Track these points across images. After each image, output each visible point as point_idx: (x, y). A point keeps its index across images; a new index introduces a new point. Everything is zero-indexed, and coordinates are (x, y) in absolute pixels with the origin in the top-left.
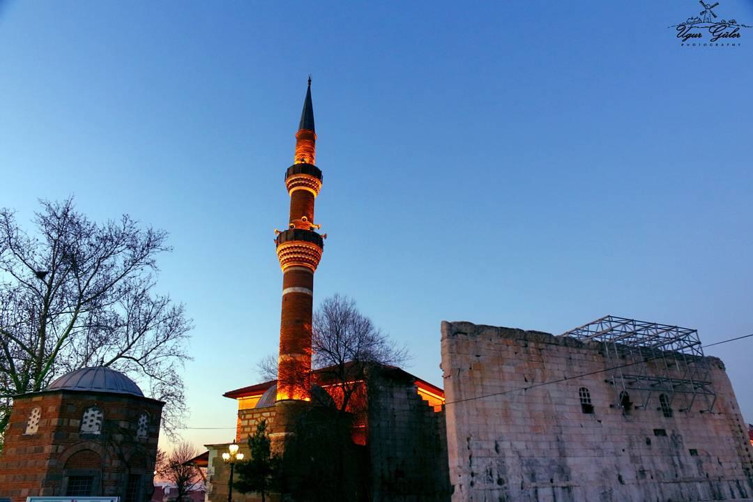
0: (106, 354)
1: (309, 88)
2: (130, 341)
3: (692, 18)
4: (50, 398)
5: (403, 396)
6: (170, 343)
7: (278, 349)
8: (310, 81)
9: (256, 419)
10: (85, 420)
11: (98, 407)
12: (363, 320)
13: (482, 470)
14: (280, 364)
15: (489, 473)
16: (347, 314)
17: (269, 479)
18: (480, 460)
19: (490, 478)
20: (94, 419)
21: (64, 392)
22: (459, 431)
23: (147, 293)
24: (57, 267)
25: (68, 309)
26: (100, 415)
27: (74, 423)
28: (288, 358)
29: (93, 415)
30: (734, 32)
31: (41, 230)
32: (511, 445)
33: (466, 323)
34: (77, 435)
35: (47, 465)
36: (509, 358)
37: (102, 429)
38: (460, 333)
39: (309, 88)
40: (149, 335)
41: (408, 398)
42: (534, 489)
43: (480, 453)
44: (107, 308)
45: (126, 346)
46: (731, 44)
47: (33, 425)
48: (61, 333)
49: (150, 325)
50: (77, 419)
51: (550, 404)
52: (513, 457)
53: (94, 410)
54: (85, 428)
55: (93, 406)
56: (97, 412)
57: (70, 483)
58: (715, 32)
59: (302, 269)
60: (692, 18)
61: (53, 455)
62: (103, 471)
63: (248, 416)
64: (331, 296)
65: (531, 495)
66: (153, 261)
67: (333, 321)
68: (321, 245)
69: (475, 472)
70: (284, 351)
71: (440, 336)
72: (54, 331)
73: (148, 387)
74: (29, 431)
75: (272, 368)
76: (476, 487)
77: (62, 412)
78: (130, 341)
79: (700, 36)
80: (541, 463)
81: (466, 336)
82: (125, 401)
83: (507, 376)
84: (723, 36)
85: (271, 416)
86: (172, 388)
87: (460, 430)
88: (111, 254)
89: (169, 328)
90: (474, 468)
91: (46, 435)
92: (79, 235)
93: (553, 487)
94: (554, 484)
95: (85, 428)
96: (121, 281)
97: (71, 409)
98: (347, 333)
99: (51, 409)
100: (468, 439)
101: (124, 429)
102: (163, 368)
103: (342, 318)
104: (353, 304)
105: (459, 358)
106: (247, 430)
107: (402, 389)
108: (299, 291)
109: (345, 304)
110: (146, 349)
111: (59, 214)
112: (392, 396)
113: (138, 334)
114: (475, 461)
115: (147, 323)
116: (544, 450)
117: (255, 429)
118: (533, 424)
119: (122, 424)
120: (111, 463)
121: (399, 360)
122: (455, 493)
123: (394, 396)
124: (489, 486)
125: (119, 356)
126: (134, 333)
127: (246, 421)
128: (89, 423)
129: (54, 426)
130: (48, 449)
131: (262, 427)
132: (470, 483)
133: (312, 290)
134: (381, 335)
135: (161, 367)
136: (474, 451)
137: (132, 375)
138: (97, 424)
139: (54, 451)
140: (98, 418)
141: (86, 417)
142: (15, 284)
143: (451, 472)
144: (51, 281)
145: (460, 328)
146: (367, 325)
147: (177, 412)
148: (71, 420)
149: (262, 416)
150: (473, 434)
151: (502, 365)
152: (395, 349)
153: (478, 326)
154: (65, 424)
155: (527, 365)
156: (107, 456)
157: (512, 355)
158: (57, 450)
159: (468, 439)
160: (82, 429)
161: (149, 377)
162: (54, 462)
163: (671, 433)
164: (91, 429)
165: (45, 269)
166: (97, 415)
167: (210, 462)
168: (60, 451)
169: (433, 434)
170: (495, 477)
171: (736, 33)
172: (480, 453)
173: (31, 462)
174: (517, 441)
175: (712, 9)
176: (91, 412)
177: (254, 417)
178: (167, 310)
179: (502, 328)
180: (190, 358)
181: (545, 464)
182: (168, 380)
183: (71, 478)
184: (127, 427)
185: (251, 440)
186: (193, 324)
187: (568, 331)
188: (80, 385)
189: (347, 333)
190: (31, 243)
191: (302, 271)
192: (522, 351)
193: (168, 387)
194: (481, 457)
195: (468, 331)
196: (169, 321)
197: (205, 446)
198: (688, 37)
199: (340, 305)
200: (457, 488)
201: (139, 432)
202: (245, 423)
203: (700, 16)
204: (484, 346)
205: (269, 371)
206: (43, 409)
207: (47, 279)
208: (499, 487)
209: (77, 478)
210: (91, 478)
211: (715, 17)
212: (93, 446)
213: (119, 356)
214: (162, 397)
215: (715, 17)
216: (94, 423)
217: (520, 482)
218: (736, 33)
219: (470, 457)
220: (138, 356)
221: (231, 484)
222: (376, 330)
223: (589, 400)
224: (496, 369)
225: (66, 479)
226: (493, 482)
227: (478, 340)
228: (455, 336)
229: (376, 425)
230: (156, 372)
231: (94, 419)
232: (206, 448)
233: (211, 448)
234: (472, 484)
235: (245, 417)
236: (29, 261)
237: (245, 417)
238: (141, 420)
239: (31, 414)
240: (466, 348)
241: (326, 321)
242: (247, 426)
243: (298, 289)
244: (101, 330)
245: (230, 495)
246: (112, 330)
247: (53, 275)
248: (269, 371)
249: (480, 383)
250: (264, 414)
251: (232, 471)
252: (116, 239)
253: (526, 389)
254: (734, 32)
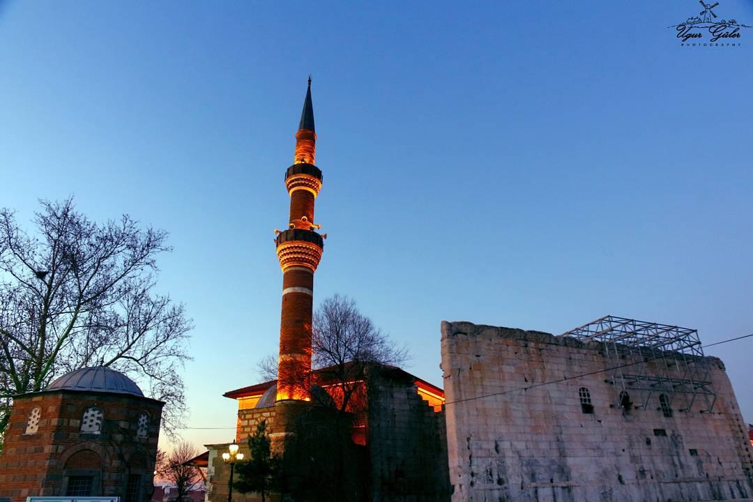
0: (106, 354)
1: (309, 88)
2: (130, 341)
3: (692, 18)
4: (50, 398)
5: (403, 396)
6: (170, 343)
7: (278, 349)
8: (310, 81)
9: (256, 419)
10: (85, 420)
11: (98, 407)
12: (363, 320)
13: (482, 470)
14: (280, 364)
15: (489, 473)
16: (347, 314)
17: (269, 479)
18: (480, 460)
19: (490, 478)
20: (94, 419)
21: (64, 392)
22: (459, 431)
23: (147, 293)
24: (57, 267)
25: (68, 309)
26: (100, 415)
27: (74, 423)
28: (288, 358)
29: (93, 415)
30: (734, 32)
31: (41, 230)
32: (511, 445)
33: (466, 323)
34: (77, 435)
35: (47, 465)
36: (509, 358)
37: (102, 429)
38: (460, 333)
39: (309, 88)
40: (149, 335)
41: (408, 398)
42: (534, 489)
43: (480, 453)
44: (107, 308)
45: (126, 346)
46: (731, 44)
47: (33, 425)
48: (61, 333)
49: (150, 325)
50: (77, 419)
51: (550, 404)
52: (513, 457)
53: (94, 410)
54: (85, 428)
55: (93, 406)
56: (97, 412)
57: (70, 483)
58: (715, 32)
59: (302, 269)
60: (692, 18)
61: (53, 455)
62: (103, 471)
63: (248, 416)
64: (331, 296)
65: (531, 495)
66: (153, 261)
67: (333, 321)
68: (321, 245)
69: (475, 472)
70: (284, 351)
71: (440, 336)
72: (54, 331)
73: (148, 387)
74: (29, 431)
75: (272, 368)
76: (476, 487)
77: (62, 412)
78: (130, 341)
79: (700, 36)
80: (541, 463)
81: (466, 336)
82: (125, 401)
83: (507, 376)
84: (723, 36)
85: (271, 416)
86: (172, 388)
87: (460, 430)
88: (111, 254)
89: (169, 328)
90: (474, 468)
91: (46, 435)
92: (79, 235)
95: (85, 428)
96: (121, 281)
97: (71, 409)
98: (347, 333)
99: (51, 409)
100: (468, 439)
101: (124, 429)
102: (163, 368)
103: (342, 318)
104: (353, 304)
105: (459, 358)
106: (247, 430)
107: (402, 389)
108: (299, 291)
109: (345, 304)
110: (146, 349)
111: (59, 214)
112: (392, 396)
113: (138, 334)
114: (475, 461)
115: (147, 323)
116: (544, 450)
117: (255, 429)
118: (533, 424)
119: (122, 424)
120: (111, 463)
121: (399, 360)
122: (455, 493)
123: (394, 396)
124: (489, 486)
125: (119, 356)
126: (134, 333)
127: (246, 421)
128: (89, 423)
129: (54, 426)
130: (48, 449)
131: (262, 427)
132: (470, 483)
133: (312, 290)
134: (381, 335)
135: (161, 367)
136: (474, 451)
137: (132, 375)
138: (97, 424)
139: (54, 451)
140: (98, 418)
141: (86, 417)
142: (15, 284)
143: (451, 472)
144: (51, 281)
145: (460, 328)
146: (367, 325)
147: (177, 412)
148: (71, 420)
149: (262, 416)
150: (473, 434)
151: (502, 365)
152: (395, 349)
153: (478, 326)
154: (65, 424)
155: (527, 365)
156: (107, 456)
157: (512, 355)
158: (57, 450)
159: (468, 439)
160: (82, 429)
161: (149, 377)
162: (54, 462)
164: (91, 429)
165: (45, 269)
166: (97, 415)
167: (210, 462)
168: (60, 451)
169: (433, 434)
170: (495, 477)
171: (736, 33)
172: (480, 453)
173: (31, 462)
174: (517, 441)
175: (712, 9)
176: (91, 412)
177: (254, 417)
178: (167, 310)
179: (502, 328)
180: (190, 358)
181: (545, 464)
182: (168, 380)
183: (71, 478)
184: (127, 427)
186: (193, 324)
187: (568, 331)
188: (80, 385)
189: (347, 333)
190: (31, 243)
191: (302, 271)
192: (522, 351)
193: (168, 387)
194: (481, 457)
195: (468, 331)
196: (169, 321)
197: (205, 446)
198: (688, 37)
199: (340, 305)
200: (457, 488)
201: (139, 432)
202: (245, 423)
203: (700, 16)
204: (484, 346)
205: (269, 371)
206: (43, 409)
207: (47, 279)
208: (499, 487)
209: (77, 478)
210: (91, 478)
211: (715, 17)
212: (93, 446)
213: (119, 356)
214: (162, 397)
215: (715, 17)
216: (94, 423)
217: (520, 482)
218: (736, 33)
219: (470, 457)
220: (138, 356)
221: (231, 484)
222: (376, 330)
223: (589, 400)
224: (496, 369)
225: (66, 479)
226: (493, 482)
227: (478, 340)
228: (455, 336)
229: (376, 425)
230: (156, 372)
231: (94, 419)
232: (206, 448)
233: (211, 448)
234: (472, 484)
235: (245, 417)
236: (29, 261)
237: (245, 417)
238: (141, 420)
239: (31, 414)
240: (466, 348)
241: (326, 321)
242: (247, 426)
243: (298, 289)
244: (101, 330)
245: (230, 495)
246: (112, 330)
247: (53, 275)
248: (269, 371)
249: (480, 383)
250: (264, 414)
251: (232, 471)
252: (116, 239)
253: (526, 389)
254: (734, 32)
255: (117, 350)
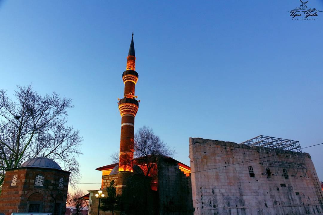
0: (46, 152)
1: (133, 38)
2: (56, 146)
3: (297, 8)
4: (22, 170)
5: (173, 170)
6: (73, 147)
7: (119, 150)
8: (133, 35)
9: (110, 179)
10: (36, 180)
11: (42, 174)
12: (156, 137)
13: (207, 201)
14: (120, 156)
15: (210, 203)
16: (149, 135)
17: (115, 205)
18: (206, 197)
19: (210, 205)
20: (41, 179)
21: (27, 168)
22: (197, 185)
23: (63, 125)
24: (25, 114)
25: (29, 132)
26: (43, 178)
27: (32, 181)
28: (124, 153)
29: (40, 178)
30: (315, 14)
31: (18, 98)
32: (219, 191)
33: (200, 138)
34: (33, 186)
35: (20, 199)
36: (218, 154)
37: (44, 184)
38: (197, 142)
39: (133, 38)
40: (64, 144)
41: (175, 171)
42: (229, 210)
43: (206, 194)
44: (46, 132)
45: (54, 148)
46: (313, 19)
47: (14, 182)
48: (26, 143)
49: (64, 139)
50: (33, 179)
51: (236, 173)
52: (220, 196)
53: (40, 176)
54: (37, 183)
55: (40, 174)
56: (42, 176)
57: (30, 207)
58: (307, 14)
59: (130, 115)
60: (297, 8)
61: (23, 195)
62: (44, 202)
63: (106, 178)
64: (142, 127)
65: (228, 212)
66: (66, 112)
67: (143, 138)
68: (138, 105)
69: (204, 202)
70: (122, 150)
71: (189, 144)
72: (23, 142)
73: (63, 166)
74: (12, 185)
75: (117, 158)
76: (204, 208)
77: (27, 177)
78: (56, 146)
79: (300, 15)
80: (232, 198)
81: (200, 144)
82: (54, 172)
83: (217, 161)
84: (310, 16)
85: (116, 178)
86: (74, 166)
87: (197, 184)
88: (48, 109)
89: (72, 140)
90: (203, 201)
91: (20, 186)
92: (34, 100)
93: (237, 209)
94: (237, 207)
95: (36, 183)
96: (52, 121)
97: (30, 175)
98: (149, 143)
99: (22, 175)
100: (201, 188)
101: (53, 184)
102: (70, 158)
103: (147, 136)
104: (151, 130)
105: (197, 153)
106: (106, 184)
107: (173, 167)
108: (128, 125)
109: (148, 130)
110: (63, 149)
111: (25, 92)
112: (168, 170)
113: (59, 143)
114: (204, 198)
115: (63, 138)
116: (233, 193)
117: (109, 184)
118: (229, 182)
119: (52, 182)
120: (48, 198)
121: (171, 154)
122: (195, 211)
123: (169, 170)
124: (210, 208)
125: (51, 152)
126: (58, 143)
127: (106, 181)
128: (38, 181)
129: (23, 183)
130: (21, 192)
131: (112, 183)
132: (201, 207)
133: (134, 124)
134: (164, 143)
135: (69, 157)
136: (203, 193)
137: (57, 161)
138: (42, 181)
139: (23, 193)
140: (42, 179)
141: (37, 179)
142: (7, 121)
143: (194, 202)
144: (22, 120)
145: (197, 140)
146: (158, 139)
147: (76, 177)
148: (31, 180)
149: (112, 178)
150: (203, 186)
151: (216, 156)
152: (169, 149)
153: (205, 140)
154: (28, 182)
155: (226, 156)
156: (46, 195)
157: (219, 152)
158: (24, 193)
159: (201, 188)
160: (35, 184)
161: (64, 161)
162: (23, 198)
163: (288, 185)
164: (39, 184)
165: (19, 115)
166: (41, 178)
167: (90, 198)
168: (26, 193)
169: (186, 186)
170: (212, 204)
171: (316, 14)
172: (206, 194)
173: (13, 198)
174: (222, 189)
175: (305, 4)
176: (39, 176)
177: (109, 179)
178: (72, 133)
179: (215, 140)
180: (82, 153)
181: (234, 199)
182: (72, 163)
183: (30, 205)
184: (54, 183)
185: (108, 188)
186: (83, 139)
187: (244, 142)
188: (34, 165)
189: (149, 143)
190: (13, 104)
191: (129, 116)
192: (224, 150)
193: (72, 166)
194: (206, 196)
195: (201, 142)
196: (72, 138)
197: (88, 191)
198: (295, 16)
199: (146, 131)
200: (196, 209)
201: (60, 185)
202: (105, 181)
203: (300, 7)
204: (208, 148)
205: (116, 159)
206: (18, 175)
207: (20, 119)
208: (214, 208)
209: (33, 205)
210: (39, 205)
211: (307, 7)
212: (40, 191)
213: (51, 152)
214: (69, 170)
215: (307, 7)
216: (40, 181)
217: (223, 206)
218: (316, 14)
219: (202, 196)
220: (59, 152)
221: (99, 207)
222: (161, 141)
223: (253, 172)
224: (213, 158)
225: (28, 205)
226: (211, 206)
227: (205, 145)
228: (195, 144)
229: (161, 182)
230: (67, 159)
231: (41, 179)
232: (88, 192)
233: (91, 192)
234: (202, 207)
235: (105, 179)
236: (13, 112)
237: (105, 179)
238: (60, 180)
239: (13, 178)
240: (200, 149)
241: (140, 137)
242: (106, 183)
243: (128, 124)
244: (43, 141)
245: (99, 212)
246: (48, 141)
247: (23, 118)
248: (116, 159)
250: (113, 177)
251: (99, 202)
252: (50, 102)
253: (225, 167)
254: (315, 14)
255: (50, 150)
